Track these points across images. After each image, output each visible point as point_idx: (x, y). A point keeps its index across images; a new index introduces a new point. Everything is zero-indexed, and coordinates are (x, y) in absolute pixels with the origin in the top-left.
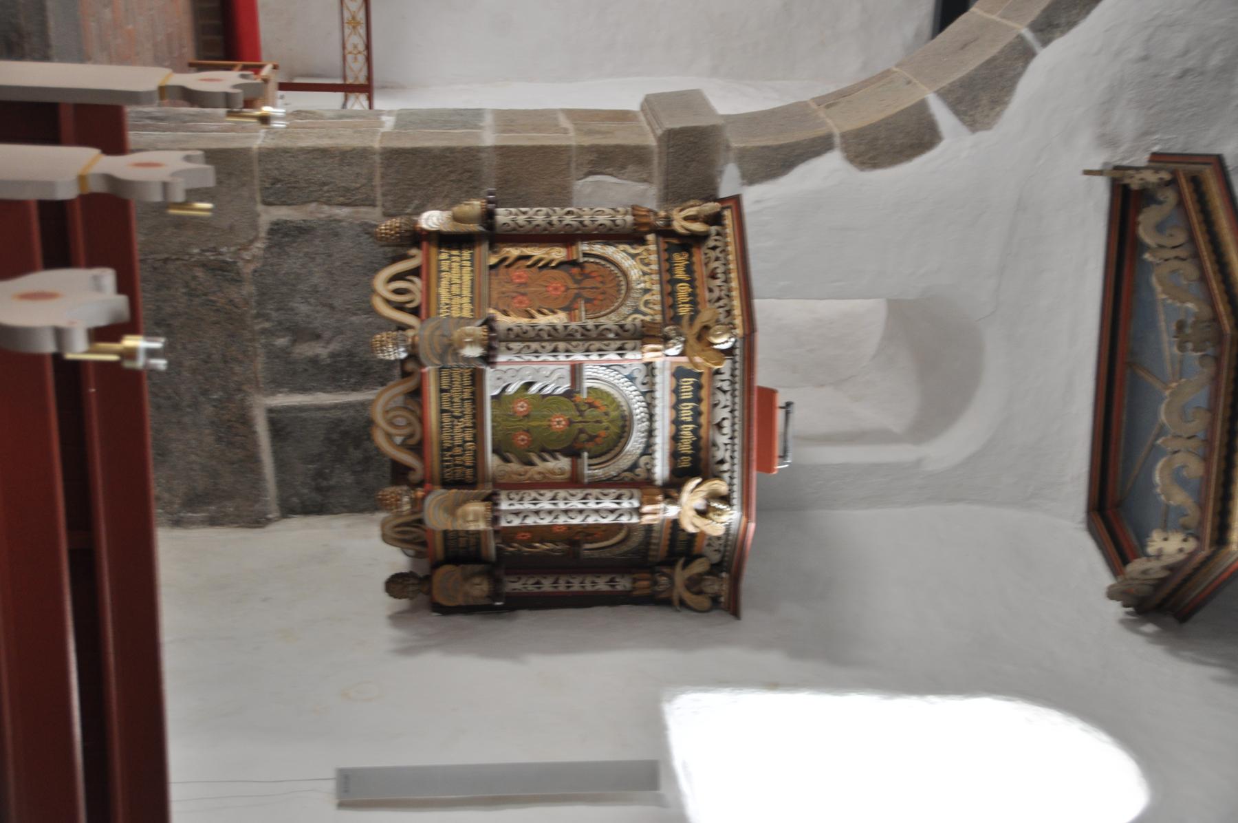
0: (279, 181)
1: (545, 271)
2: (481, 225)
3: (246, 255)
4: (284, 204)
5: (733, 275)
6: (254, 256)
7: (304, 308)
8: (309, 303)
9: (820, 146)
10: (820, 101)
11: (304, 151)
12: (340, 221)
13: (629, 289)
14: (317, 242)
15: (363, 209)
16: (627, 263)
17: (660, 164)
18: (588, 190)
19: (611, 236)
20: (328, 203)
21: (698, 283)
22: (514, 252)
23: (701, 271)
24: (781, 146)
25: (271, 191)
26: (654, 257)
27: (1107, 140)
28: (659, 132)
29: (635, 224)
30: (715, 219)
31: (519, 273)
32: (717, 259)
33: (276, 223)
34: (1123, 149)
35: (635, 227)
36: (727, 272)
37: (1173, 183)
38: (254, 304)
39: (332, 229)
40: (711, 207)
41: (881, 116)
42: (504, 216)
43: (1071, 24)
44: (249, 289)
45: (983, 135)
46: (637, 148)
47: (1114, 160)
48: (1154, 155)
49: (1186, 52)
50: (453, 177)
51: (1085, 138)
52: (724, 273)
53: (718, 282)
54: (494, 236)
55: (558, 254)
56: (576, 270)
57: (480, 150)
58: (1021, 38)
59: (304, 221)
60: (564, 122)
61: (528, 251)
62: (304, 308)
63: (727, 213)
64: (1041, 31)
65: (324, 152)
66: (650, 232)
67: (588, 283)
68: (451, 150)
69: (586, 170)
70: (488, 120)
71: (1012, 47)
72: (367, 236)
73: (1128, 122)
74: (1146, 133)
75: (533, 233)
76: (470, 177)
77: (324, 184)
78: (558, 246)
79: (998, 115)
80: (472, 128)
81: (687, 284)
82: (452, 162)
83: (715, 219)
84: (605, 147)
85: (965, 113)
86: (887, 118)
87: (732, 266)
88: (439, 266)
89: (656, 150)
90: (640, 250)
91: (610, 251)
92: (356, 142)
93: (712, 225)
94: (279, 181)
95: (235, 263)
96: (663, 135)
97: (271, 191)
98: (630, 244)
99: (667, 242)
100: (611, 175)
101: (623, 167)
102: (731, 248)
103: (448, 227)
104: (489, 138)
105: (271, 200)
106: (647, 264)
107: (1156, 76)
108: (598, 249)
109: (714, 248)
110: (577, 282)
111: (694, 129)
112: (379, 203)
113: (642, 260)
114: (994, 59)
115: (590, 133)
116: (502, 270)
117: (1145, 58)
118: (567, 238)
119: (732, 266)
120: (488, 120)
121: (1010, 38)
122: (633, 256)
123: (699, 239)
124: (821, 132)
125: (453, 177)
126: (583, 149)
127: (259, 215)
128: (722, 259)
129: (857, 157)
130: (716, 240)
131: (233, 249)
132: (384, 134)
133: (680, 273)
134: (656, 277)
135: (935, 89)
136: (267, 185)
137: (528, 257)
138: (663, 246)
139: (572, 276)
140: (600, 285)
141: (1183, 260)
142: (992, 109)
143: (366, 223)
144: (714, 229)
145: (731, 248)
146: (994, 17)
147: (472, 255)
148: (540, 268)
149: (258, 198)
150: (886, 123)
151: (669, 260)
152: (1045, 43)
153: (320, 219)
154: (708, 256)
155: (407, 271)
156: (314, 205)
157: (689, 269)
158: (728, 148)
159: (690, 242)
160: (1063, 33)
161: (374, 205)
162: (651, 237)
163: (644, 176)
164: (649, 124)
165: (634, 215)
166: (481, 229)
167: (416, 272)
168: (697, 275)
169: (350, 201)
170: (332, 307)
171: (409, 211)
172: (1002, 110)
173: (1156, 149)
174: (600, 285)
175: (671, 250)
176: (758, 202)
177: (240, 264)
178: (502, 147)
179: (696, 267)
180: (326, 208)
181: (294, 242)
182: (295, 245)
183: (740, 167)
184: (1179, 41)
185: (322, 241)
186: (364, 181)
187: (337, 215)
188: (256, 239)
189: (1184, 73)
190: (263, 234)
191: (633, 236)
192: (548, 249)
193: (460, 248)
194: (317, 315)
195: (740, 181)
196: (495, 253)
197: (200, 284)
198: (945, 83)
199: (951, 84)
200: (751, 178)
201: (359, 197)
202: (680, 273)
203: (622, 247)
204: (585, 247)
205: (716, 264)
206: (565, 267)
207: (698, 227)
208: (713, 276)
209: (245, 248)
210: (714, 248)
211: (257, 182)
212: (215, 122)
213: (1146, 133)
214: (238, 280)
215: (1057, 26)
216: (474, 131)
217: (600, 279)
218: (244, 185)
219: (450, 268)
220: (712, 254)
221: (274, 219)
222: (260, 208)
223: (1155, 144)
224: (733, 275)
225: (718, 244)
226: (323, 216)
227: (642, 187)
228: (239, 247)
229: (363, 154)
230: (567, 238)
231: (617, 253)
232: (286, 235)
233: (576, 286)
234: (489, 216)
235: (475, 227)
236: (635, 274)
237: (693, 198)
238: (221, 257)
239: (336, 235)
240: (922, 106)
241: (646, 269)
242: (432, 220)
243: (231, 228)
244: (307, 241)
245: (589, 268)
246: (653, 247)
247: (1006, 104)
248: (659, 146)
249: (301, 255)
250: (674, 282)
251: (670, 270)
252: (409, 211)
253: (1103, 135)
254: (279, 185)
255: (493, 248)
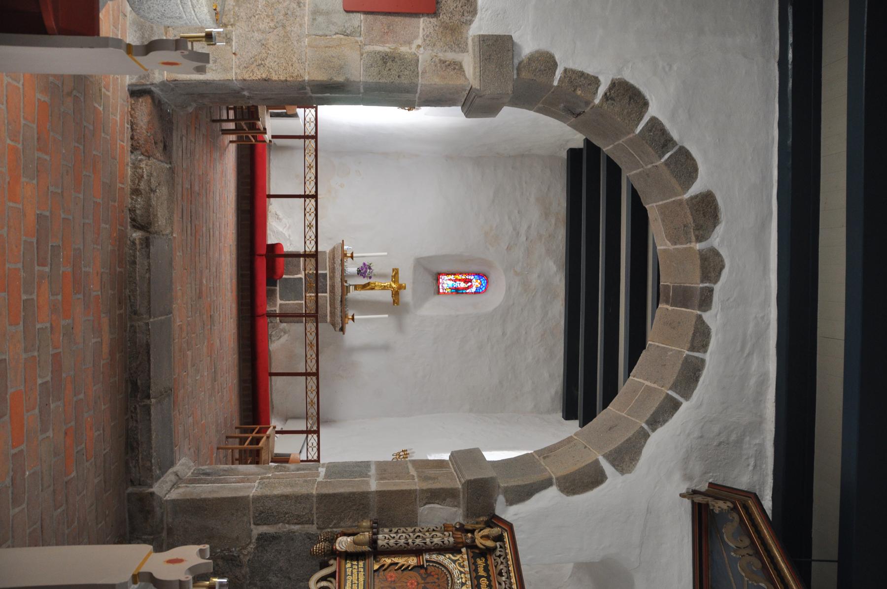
0: (263, 512)
1: (405, 572)
2: (369, 547)
3: (245, 552)
4: (265, 524)
5: (512, 574)
6: (249, 552)
7: (274, 579)
8: (277, 577)
9: (546, 484)
10: (540, 452)
11: (275, 496)
12: (294, 532)
13: (453, 583)
14: (282, 543)
15: (306, 526)
16: (451, 566)
17: (463, 498)
18: (426, 512)
19: (441, 550)
20: (288, 523)
21: (492, 578)
22: (388, 561)
23: (493, 571)
24: (526, 485)
25: (258, 518)
26: (466, 563)
27: (688, 477)
28: (463, 481)
29: (454, 543)
30: (499, 538)
31: (392, 574)
32: (502, 563)
33: (261, 535)
34: (695, 481)
35: (455, 545)
36: (508, 572)
37: (735, 508)
38: (248, 577)
39: (290, 537)
40: (496, 531)
41: (576, 468)
42: (383, 539)
43: (665, 421)
44: (246, 570)
45: (627, 476)
46: (452, 489)
47: (692, 487)
48: (710, 483)
49: (720, 434)
50: (354, 508)
51: (677, 476)
52: (506, 572)
53: (504, 579)
54: (375, 551)
55: (412, 561)
56: (423, 571)
57: (368, 493)
58: (642, 427)
59: (276, 533)
60: (413, 471)
61: (396, 560)
62: (274, 579)
63: (505, 534)
64: (651, 424)
65: (287, 497)
66: (463, 547)
67: (429, 579)
68: (354, 494)
69: (424, 502)
70: (373, 471)
71: (638, 432)
72: (309, 540)
73: (697, 468)
74: (705, 473)
75: (398, 549)
76: (363, 507)
77: (286, 513)
78: (412, 556)
79: (634, 466)
80: (364, 477)
81: (485, 579)
82: (354, 500)
83: (499, 538)
84: (436, 489)
85: (618, 466)
86: (579, 469)
87: (511, 568)
88: (346, 571)
89: (461, 490)
90: (458, 557)
91: (441, 558)
92: (304, 491)
93: (496, 542)
94: (263, 512)
95: (239, 556)
96: (465, 483)
97: (258, 518)
98: (452, 554)
99: (472, 552)
100: (438, 504)
101: (445, 499)
102: (509, 557)
103: (351, 549)
104: (373, 485)
105: (258, 522)
106: (463, 567)
107: (707, 445)
108: (434, 557)
109: (500, 556)
110: (424, 579)
111: (482, 479)
112: (315, 523)
113: (459, 564)
114: (630, 439)
115: (426, 479)
116: (381, 573)
117: (701, 437)
118: (418, 552)
119: (511, 568)
120: (373, 471)
121: (637, 428)
122: (454, 562)
123: (491, 551)
124: (545, 476)
125: (354, 508)
126: (423, 491)
127: (252, 531)
128: (504, 563)
129: (565, 489)
130: (500, 551)
131: (237, 549)
132: (320, 483)
133: (482, 572)
134: (468, 576)
135: (602, 454)
136: (257, 515)
137: (397, 564)
138: (471, 554)
139: (421, 575)
140: (437, 581)
141: (751, 555)
142: (631, 463)
143: (308, 533)
144: (498, 544)
145: (509, 557)
146: (623, 414)
147: (364, 564)
148: (402, 571)
149: (252, 522)
150: (579, 471)
151: (475, 563)
152: (654, 430)
153: (284, 532)
154: (496, 561)
155: (328, 575)
156: (281, 524)
157: (486, 569)
158: (499, 487)
159: (486, 552)
160: (661, 425)
161: (313, 524)
162: (464, 550)
163: (456, 504)
164: (455, 471)
165: (454, 538)
166: (369, 549)
167: (333, 575)
168: (491, 573)
169: (300, 522)
170: (290, 578)
171: (331, 526)
172: (636, 464)
173: (711, 481)
174: (437, 581)
175: (475, 557)
176: (515, 515)
177: (242, 556)
178: (380, 491)
179: (490, 568)
180: (287, 526)
181: (270, 544)
182: (270, 546)
183: (505, 496)
184: (716, 429)
185: (284, 543)
186: (308, 511)
187: (293, 529)
188: (250, 542)
189: (720, 444)
190: (254, 541)
191: (455, 550)
192: (406, 558)
193: (358, 560)
194: (281, 583)
195: (505, 504)
196: (377, 562)
197: (220, 568)
198: (607, 451)
199: (610, 451)
200: (511, 502)
201: (304, 519)
202: (482, 572)
203: (447, 556)
204: (427, 557)
205: (501, 567)
206: (417, 569)
207: (490, 543)
208: (500, 574)
209: (244, 548)
210: (500, 556)
211: (251, 513)
212: (235, 475)
213: (705, 473)
214: (240, 565)
215: (659, 422)
216: (365, 479)
217: (436, 576)
218: (244, 515)
219: (352, 572)
220: (499, 560)
221: (260, 532)
222: (253, 526)
223: (710, 478)
224: (512, 574)
225: (501, 553)
226: (285, 530)
227: (455, 509)
228: (241, 548)
229: (308, 497)
230: (418, 552)
231: (445, 559)
232: (266, 540)
233: (423, 582)
234: (373, 542)
235: (366, 548)
236: (456, 573)
237: (482, 516)
238: (231, 554)
239: (293, 539)
240: (597, 462)
241: (462, 569)
242: (343, 543)
243: (237, 538)
244: (277, 543)
245: (430, 569)
246: (465, 556)
247: (638, 460)
248: (463, 489)
249: (274, 551)
250: (478, 578)
251: (476, 570)
252: (331, 526)
253: (686, 474)
254: (263, 515)
255: (376, 559)
